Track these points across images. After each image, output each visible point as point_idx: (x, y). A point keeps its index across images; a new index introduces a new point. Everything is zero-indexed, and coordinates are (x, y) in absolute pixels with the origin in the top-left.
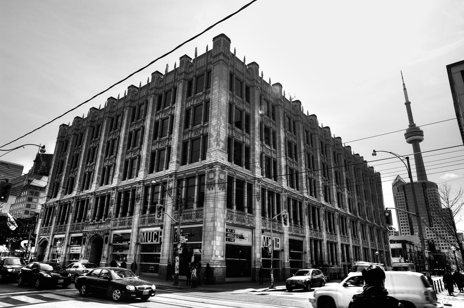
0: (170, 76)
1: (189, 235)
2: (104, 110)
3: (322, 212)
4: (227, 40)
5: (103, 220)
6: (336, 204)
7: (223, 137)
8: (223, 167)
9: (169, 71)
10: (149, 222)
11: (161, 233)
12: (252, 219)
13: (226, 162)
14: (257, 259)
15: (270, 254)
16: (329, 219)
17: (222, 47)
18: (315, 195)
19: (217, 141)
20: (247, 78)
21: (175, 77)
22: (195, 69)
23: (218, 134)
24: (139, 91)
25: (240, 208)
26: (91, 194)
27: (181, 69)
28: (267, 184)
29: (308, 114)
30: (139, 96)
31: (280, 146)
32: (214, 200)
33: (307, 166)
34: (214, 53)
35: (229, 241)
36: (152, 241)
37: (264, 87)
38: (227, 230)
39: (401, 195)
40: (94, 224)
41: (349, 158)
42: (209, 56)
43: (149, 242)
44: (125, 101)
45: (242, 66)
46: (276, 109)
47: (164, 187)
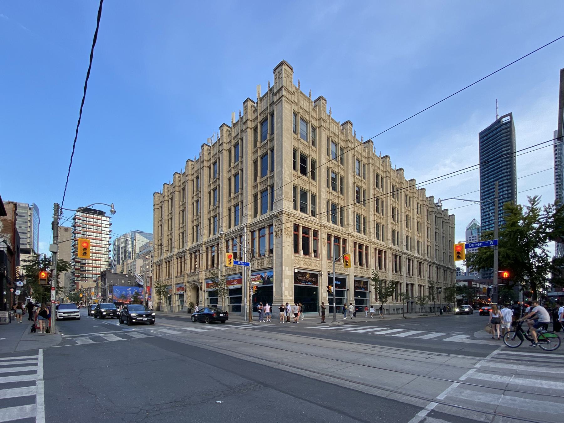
3: (389, 255)
4: (289, 68)
6: (416, 252)
14: (324, 297)
16: (360, 253)
25: (361, 264)
28: (358, 238)
37: (333, 127)
39: (474, 238)
45: (307, 103)
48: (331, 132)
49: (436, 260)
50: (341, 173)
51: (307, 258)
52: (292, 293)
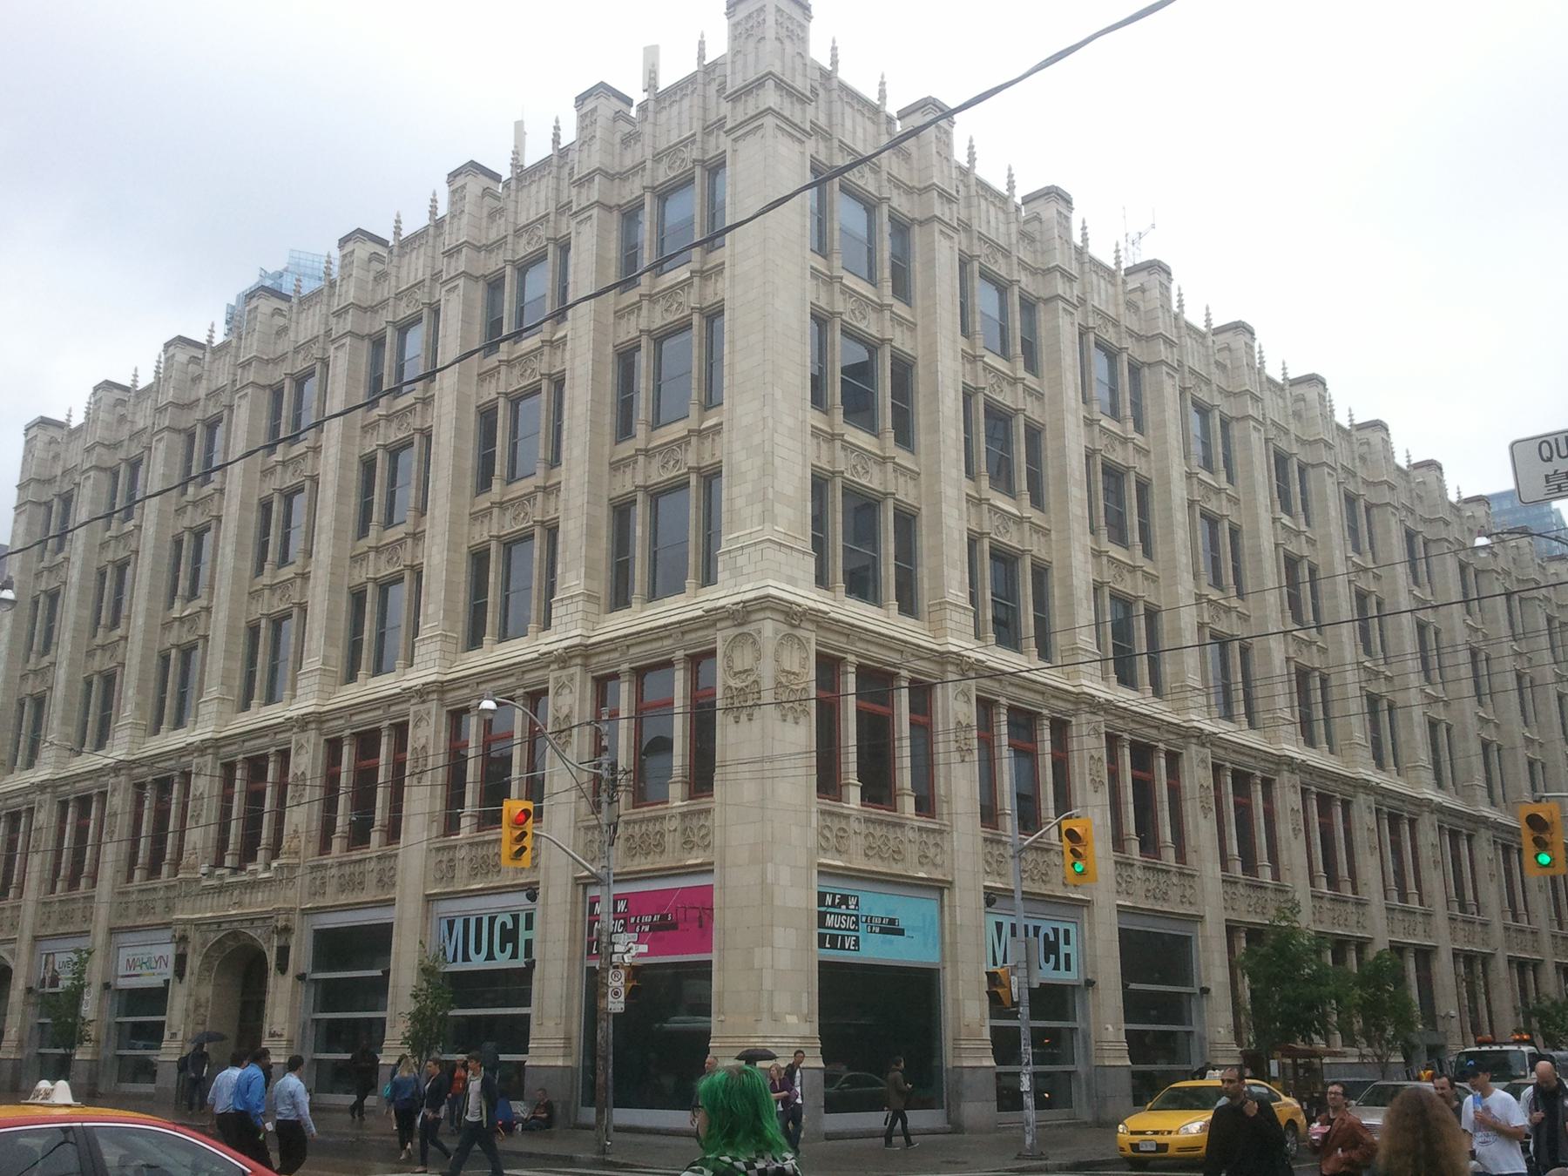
0: (534, 188)
1: (654, 927)
2: (233, 351)
5: (260, 867)
7: (793, 484)
8: (792, 615)
9: (529, 160)
10: (474, 873)
11: (529, 918)
12: (936, 845)
13: (807, 595)
15: (1016, 1005)
16: (1144, 790)
17: (770, 45)
18: (1250, 713)
19: (765, 498)
20: (897, 183)
21: (557, 190)
22: (649, 153)
23: (768, 470)
24: (395, 260)
25: (878, 789)
26: (198, 749)
27: (585, 154)
29: (1208, 321)
30: (393, 283)
31: (1064, 496)
32: (759, 775)
33: (1206, 578)
34: (733, 73)
35: (834, 947)
36: (490, 956)
38: (822, 896)
40: (221, 889)
41: (1431, 521)
42: (714, 87)
43: (478, 963)
44: (328, 305)
45: (869, 124)
46: (1042, 315)
47: (536, 724)
48: (1123, 329)
49: (1493, 803)
50: (1029, 408)
51: (881, 822)
52: (809, 999)
